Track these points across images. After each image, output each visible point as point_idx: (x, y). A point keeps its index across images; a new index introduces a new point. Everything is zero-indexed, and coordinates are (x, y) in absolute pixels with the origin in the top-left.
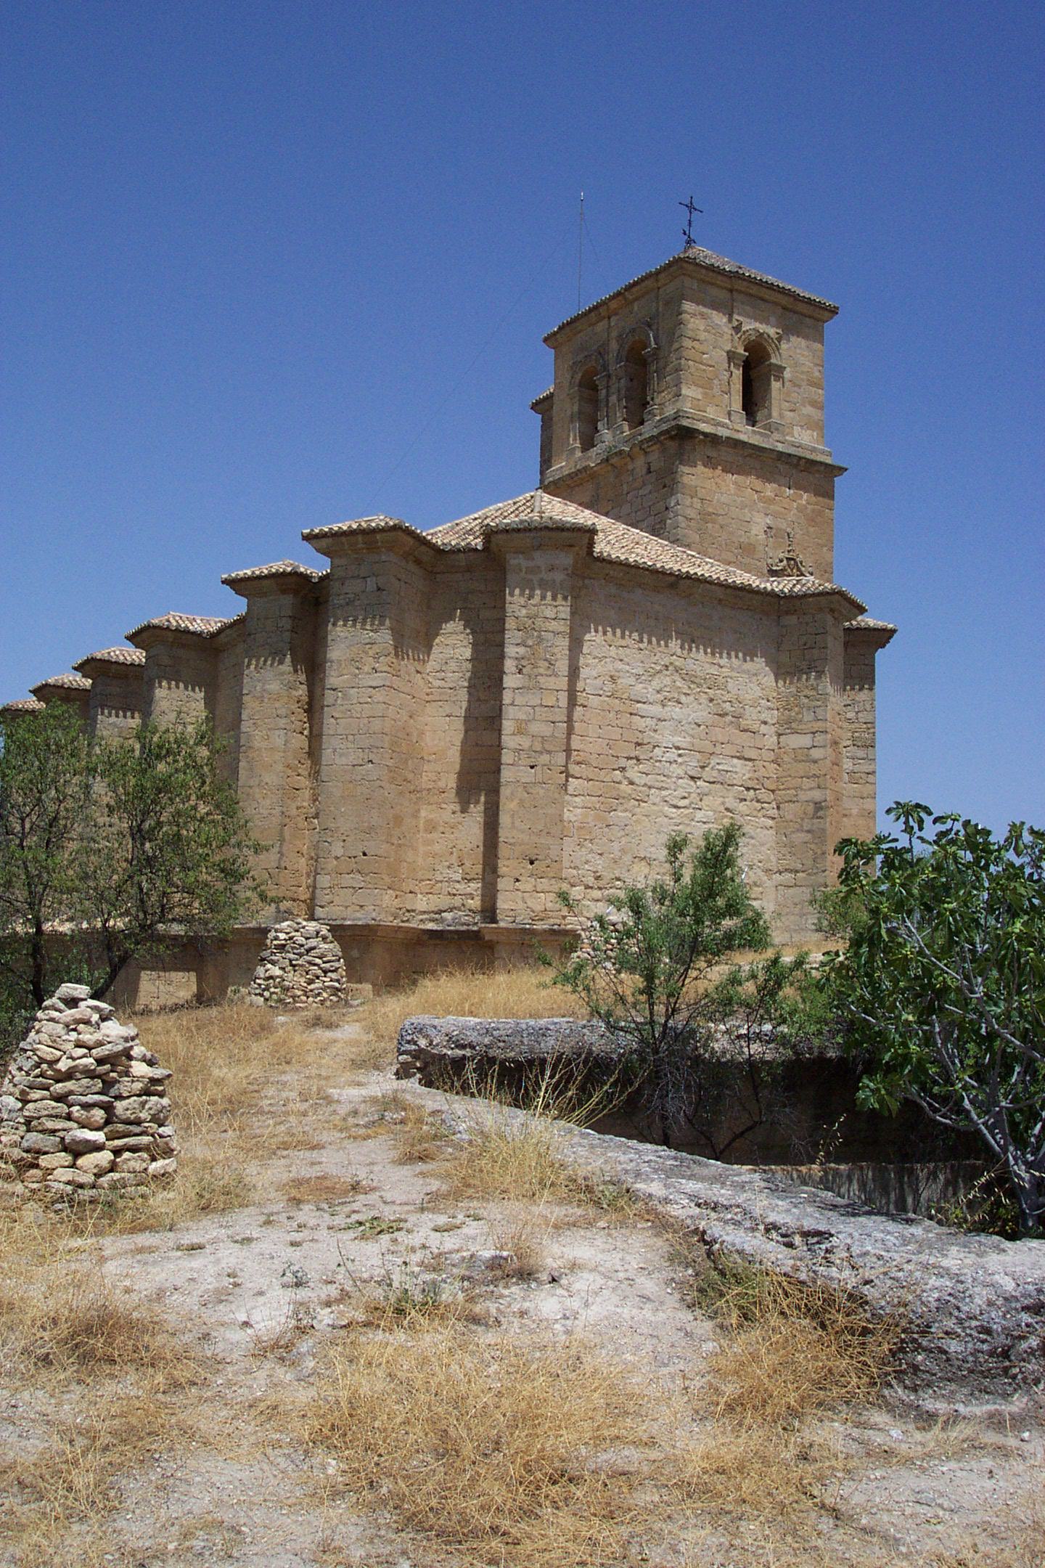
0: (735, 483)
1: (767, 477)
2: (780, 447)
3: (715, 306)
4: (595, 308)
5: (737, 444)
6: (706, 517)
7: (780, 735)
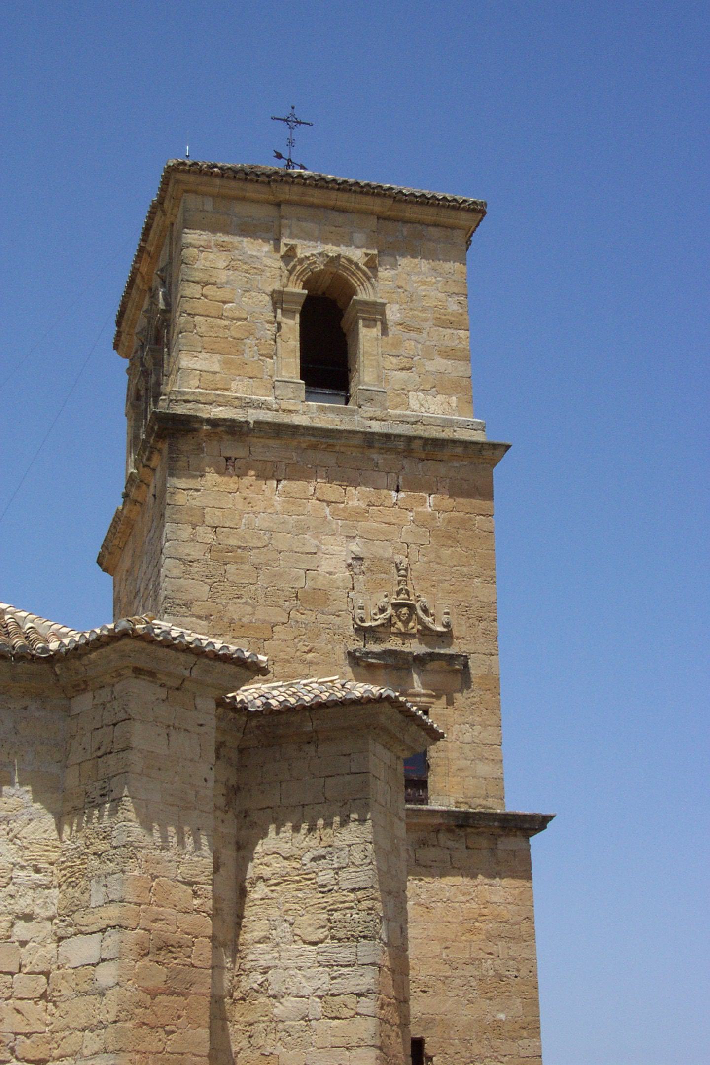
0: (286, 494)
1: (348, 476)
2: (376, 427)
3: (247, 230)
4: (131, 283)
5: (279, 430)
6: (223, 555)
7: (61, 939)
